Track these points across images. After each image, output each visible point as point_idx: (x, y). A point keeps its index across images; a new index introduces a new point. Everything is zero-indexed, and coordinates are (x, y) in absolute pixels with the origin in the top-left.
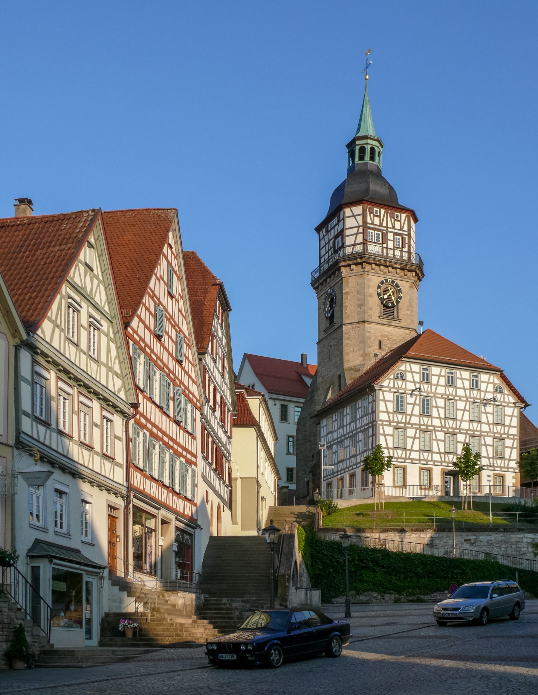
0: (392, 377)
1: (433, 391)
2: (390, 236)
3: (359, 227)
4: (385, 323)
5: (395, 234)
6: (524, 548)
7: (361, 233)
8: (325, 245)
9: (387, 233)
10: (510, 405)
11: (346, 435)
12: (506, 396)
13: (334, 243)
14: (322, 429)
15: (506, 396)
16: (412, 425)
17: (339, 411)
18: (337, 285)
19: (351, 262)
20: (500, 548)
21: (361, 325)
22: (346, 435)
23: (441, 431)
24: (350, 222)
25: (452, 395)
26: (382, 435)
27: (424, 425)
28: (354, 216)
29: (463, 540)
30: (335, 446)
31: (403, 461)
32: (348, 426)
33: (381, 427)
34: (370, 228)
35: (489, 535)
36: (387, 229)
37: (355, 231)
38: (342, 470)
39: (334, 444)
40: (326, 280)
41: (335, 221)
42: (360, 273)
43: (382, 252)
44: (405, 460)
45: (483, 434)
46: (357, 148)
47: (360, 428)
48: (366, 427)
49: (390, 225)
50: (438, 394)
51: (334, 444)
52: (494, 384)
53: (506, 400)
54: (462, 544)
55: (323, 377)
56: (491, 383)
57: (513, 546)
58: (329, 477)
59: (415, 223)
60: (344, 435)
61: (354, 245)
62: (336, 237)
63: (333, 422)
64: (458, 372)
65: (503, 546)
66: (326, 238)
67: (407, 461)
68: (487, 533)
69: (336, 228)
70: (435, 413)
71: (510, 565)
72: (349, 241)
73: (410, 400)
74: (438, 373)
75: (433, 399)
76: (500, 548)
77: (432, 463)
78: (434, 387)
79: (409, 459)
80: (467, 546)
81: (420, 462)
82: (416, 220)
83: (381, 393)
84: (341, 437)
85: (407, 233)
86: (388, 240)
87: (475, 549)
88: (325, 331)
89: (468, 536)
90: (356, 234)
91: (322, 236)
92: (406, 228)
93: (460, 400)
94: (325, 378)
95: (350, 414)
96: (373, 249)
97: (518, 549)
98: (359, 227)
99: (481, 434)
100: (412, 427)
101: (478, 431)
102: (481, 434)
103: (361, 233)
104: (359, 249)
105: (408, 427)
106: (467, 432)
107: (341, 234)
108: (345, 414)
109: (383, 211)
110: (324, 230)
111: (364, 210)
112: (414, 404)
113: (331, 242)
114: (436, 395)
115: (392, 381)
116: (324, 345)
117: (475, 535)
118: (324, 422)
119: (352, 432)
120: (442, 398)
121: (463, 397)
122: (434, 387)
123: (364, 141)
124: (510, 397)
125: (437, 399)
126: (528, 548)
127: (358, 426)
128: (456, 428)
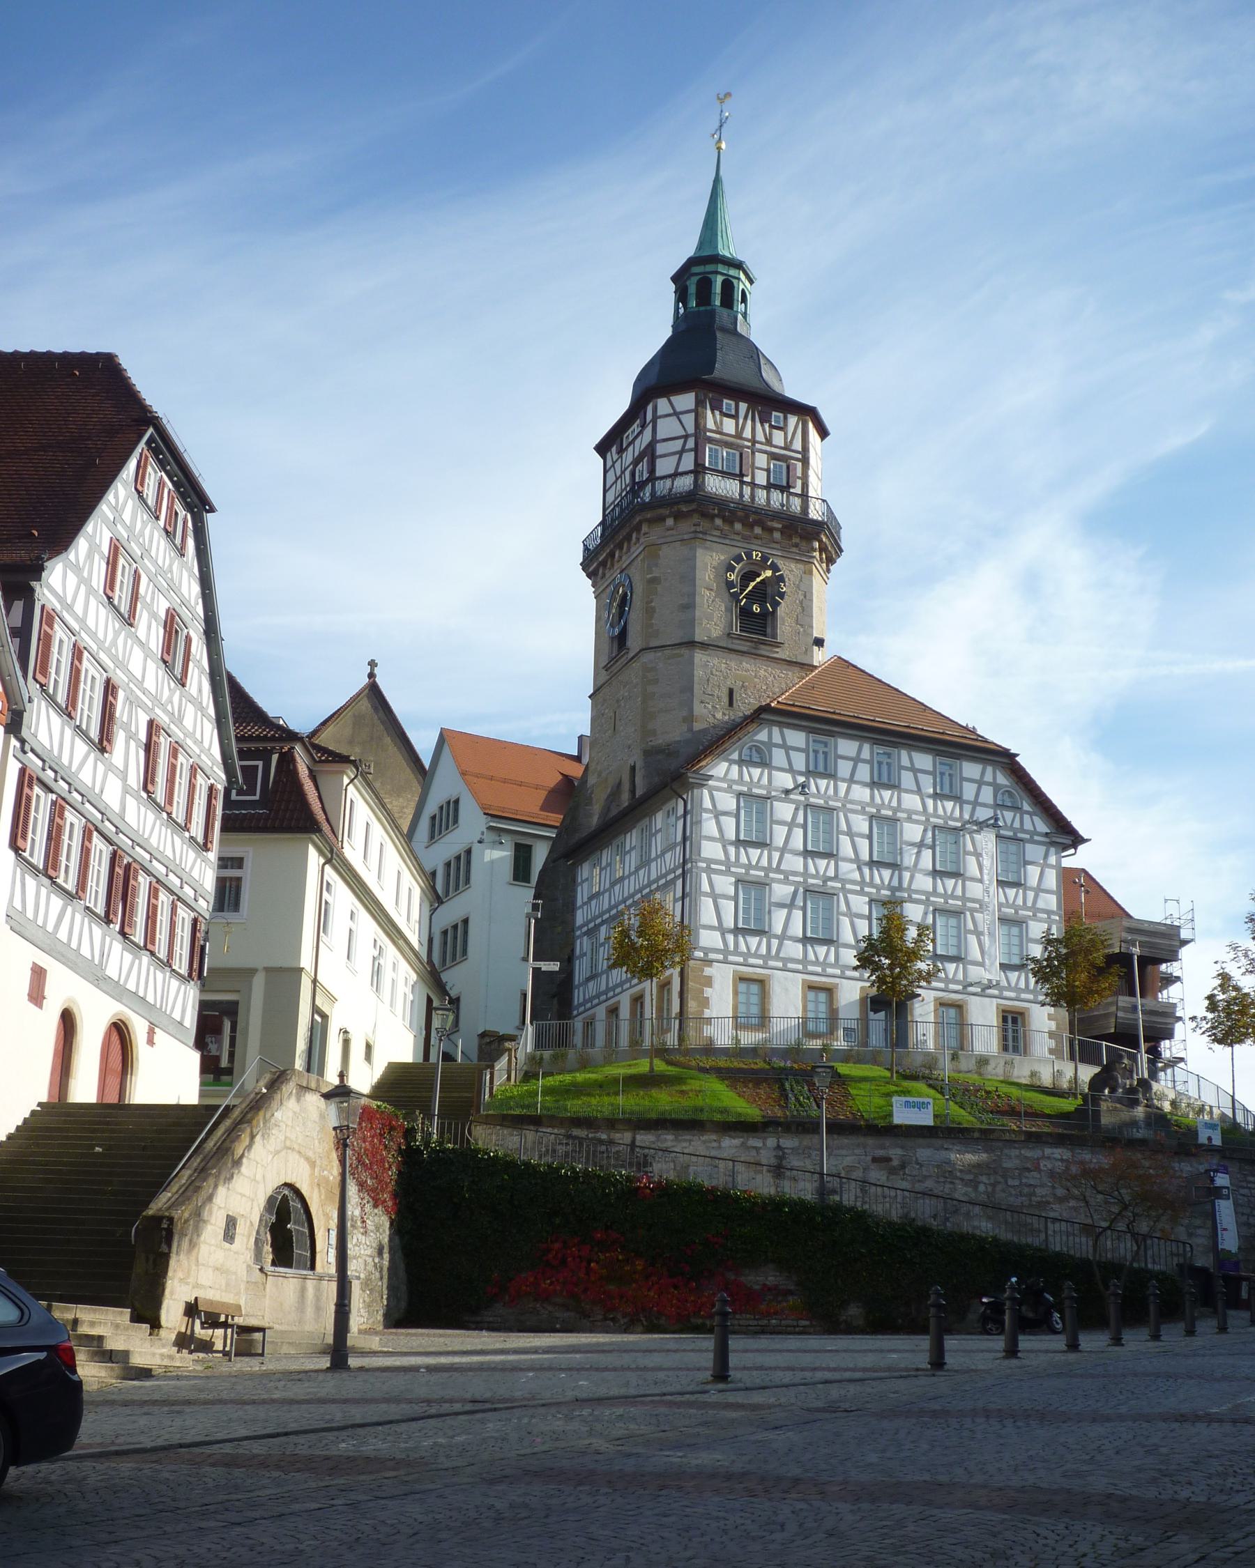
0: (735, 756)
1: (842, 793)
2: (761, 460)
3: (686, 437)
4: (745, 649)
5: (773, 456)
6: (1042, 1186)
7: (691, 450)
8: (616, 482)
9: (753, 453)
10: (1036, 838)
11: (628, 898)
12: (1026, 817)
13: (633, 474)
14: (579, 889)
15: (1026, 817)
16: (787, 874)
17: (615, 843)
18: (635, 563)
19: (666, 512)
20: (975, 1184)
21: (684, 651)
22: (628, 898)
23: (861, 893)
24: (667, 427)
26: (706, 895)
27: (816, 876)
28: (676, 414)
29: (869, 1158)
30: (603, 929)
31: (760, 962)
32: (632, 878)
33: (704, 876)
34: (711, 440)
35: (942, 1148)
36: (753, 445)
37: (678, 445)
38: (617, 986)
39: (603, 923)
40: (612, 555)
41: (636, 427)
42: (686, 537)
43: (741, 495)
44: (765, 962)
45: (969, 904)
46: (695, 279)
47: (656, 881)
48: (669, 878)
49: (760, 437)
50: (852, 802)
51: (603, 923)
52: (997, 788)
53: (1028, 825)
55: (599, 775)
56: (989, 784)
57: (1010, 1182)
58: (589, 1005)
59: (822, 439)
60: (624, 901)
61: (676, 474)
62: (636, 462)
63: (601, 870)
64: (904, 753)
65: (984, 1179)
66: (618, 465)
67: (771, 963)
68: (939, 1142)
69: (637, 442)
71: (1005, 1235)
72: (664, 467)
73: (784, 810)
74: (853, 754)
75: (841, 815)
76: (975, 1184)
77: (838, 972)
79: (777, 958)
80: (877, 1175)
81: (805, 967)
82: (823, 433)
83: (705, 792)
84: (616, 906)
85: (800, 456)
86: (753, 467)
87: (905, 1185)
88: (606, 668)
89: (883, 1147)
90: (681, 453)
91: (609, 463)
92: (797, 445)
93: (909, 819)
94: (604, 775)
95: (638, 849)
96: (716, 485)
97: (1026, 1190)
98: (686, 437)
99: (964, 905)
100: (786, 881)
101: (956, 898)
103: (691, 450)
105: (774, 880)
106: (928, 899)
107: (650, 453)
108: (628, 848)
109: (743, 406)
110: (614, 449)
111: (699, 403)
113: (627, 473)
114: (849, 806)
116: (605, 700)
117: (902, 1147)
118: (584, 871)
119: (640, 891)
120: (863, 812)
121: (917, 813)
123: (709, 268)
124: (1037, 820)
125: (851, 816)
126: (1053, 1187)
127: (653, 876)
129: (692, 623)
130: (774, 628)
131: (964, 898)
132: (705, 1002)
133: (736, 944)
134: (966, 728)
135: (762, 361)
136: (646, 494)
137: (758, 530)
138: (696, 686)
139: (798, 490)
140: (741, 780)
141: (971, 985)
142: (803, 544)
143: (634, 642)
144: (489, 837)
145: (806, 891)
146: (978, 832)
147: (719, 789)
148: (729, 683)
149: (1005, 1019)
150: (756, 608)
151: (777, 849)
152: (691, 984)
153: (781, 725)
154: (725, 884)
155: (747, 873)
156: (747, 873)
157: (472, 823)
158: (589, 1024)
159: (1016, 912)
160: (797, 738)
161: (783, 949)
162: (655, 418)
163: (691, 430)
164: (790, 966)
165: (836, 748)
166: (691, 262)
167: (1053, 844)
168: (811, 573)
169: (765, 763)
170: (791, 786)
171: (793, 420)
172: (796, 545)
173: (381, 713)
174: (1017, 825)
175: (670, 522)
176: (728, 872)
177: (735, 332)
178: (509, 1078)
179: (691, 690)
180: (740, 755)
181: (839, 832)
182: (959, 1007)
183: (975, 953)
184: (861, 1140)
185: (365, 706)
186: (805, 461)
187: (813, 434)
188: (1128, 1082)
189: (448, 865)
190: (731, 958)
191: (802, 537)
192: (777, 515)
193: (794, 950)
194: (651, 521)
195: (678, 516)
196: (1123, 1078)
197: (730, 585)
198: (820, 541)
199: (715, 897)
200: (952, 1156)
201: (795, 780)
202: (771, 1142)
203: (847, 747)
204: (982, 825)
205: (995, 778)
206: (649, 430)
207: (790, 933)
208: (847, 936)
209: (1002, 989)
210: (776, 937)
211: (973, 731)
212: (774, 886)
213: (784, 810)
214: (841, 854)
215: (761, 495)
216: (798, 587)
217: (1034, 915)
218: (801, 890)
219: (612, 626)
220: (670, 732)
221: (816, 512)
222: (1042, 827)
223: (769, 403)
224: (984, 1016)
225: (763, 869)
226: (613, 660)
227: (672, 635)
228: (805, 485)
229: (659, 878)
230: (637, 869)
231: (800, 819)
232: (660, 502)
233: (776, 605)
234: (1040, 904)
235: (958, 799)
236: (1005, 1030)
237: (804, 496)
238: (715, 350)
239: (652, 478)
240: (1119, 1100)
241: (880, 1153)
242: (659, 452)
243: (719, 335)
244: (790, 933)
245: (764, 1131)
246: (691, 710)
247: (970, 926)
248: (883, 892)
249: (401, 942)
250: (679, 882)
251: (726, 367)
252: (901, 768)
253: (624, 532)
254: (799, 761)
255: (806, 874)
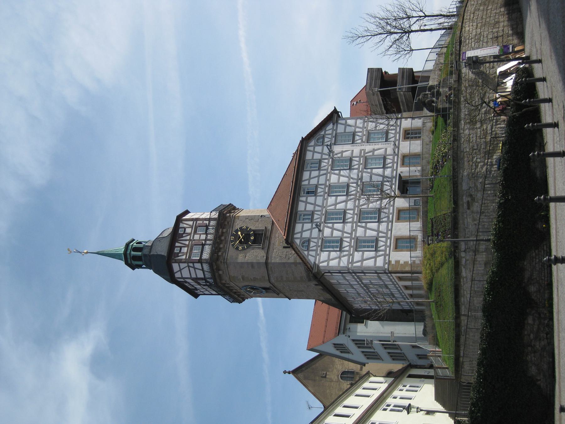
0: (306, 253)
1: (320, 208)
2: (197, 237)
5: (195, 232)
6: (476, 133)
9: (194, 240)
13: (204, 285)
15: (327, 132)
16: (353, 230)
19: (217, 275)
21: (270, 266)
25: (325, 188)
26: (362, 264)
27: (353, 218)
28: (180, 270)
29: (468, 211)
31: (389, 240)
33: (354, 265)
34: (190, 257)
40: (235, 293)
42: (226, 266)
44: (389, 238)
47: (358, 282)
49: (188, 238)
50: (323, 204)
54: (473, 212)
56: (314, 148)
61: (203, 270)
62: (200, 284)
64: (303, 183)
66: (202, 290)
67: (389, 236)
70: (341, 206)
72: (200, 275)
73: (327, 232)
78: (317, 208)
79: (387, 233)
80: (476, 207)
82: (187, 212)
86: (199, 240)
88: (278, 294)
90: (195, 268)
91: (201, 293)
93: (329, 180)
98: (189, 266)
99: (362, 157)
100: (356, 230)
101: (360, 160)
102: (362, 157)
104: (206, 267)
105: (355, 236)
106: (361, 172)
107: (196, 280)
109: (177, 244)
112: (333, 229)
115: (311, 253)
118: (356, 306)
119: (362, 287)
122: (317, 208)
123: (128, 257)
125: (329, 204)
127: (356, 283)
128: (357, 183)
129: (258, 263)
130: (259, 230)
131: (360, 157)
132: (406, 263)
133: (382, 251)
134: (293, 157)
135: (161, 236)
136: (211, 281)
137: (223, 238)
138: (283, 261)
139: (207, 222)
140: (316, 251)
141: (395, 152)
142: (228, 220)
143: (267, 285)
144: (348, 333)
145: (359, 222)
146: (333, 152)
147: (319, 259)
148: (281, 248)
149: (408, 138)
150: (252, 238)
151: (343, 235)
152: (399, 269)
153: (293, 234)
154: (357, 256)
155: (353, 247)
156: (353, 247)
157: (342, 339)
158: (418, 304)
159: (365, 135)
160: (298, 228)
161: (383, 231)
162: (182, 278)
163: (186, 265)
164: (390, 228)
165: (301, 211)
166: (127, 263)
167: (337, 122)
168: (238, 216)
169: (309, 241)
170: (317, 230)
171: (181, 225)
172: (228, 223)
173: (303, 369)
174: (330, 136)
175: (221, 272)
176: (353, 255)
177: (152, 246)
178: (440, 356)
179: (284, 263)
180: (305, 251)
181: (335, 209)
182: (404, 157)
183: (381, 152)
184: (460, 214)
185: (301, 375)
186: (197, 220)
187: (188, 216)
188: (429, 96)
189: (359, 347)
190: (388, 253)
191: (225, 221)
192: (217, 231)
193: (383, 227)
194: (221, 280)
195: (218, 269)
196: (427, 98)
197: (244, 249)
198: (227, 213)
199: (363, 260)
200: (465, 174)
201: (314, 228)
202: (463, 254)
203: (301, 207)
204: (331, 151)
205: (311, 146)
206: (187, 280)
207: (376, 228)
208: (376, 205)
209: (396, 140)
210: (378, 234)
211: (294, 154)
212: (357, 235)
213: (327, 232)
214: (344, 208)
215: (210, 237)
216: (244, 221)
217: (365, 128)
218: (359, 224)
219: (262, 292)
220: (301, 271)
221: (215, 215)
222: (330, 126)
223: (176, 234)
224: (406, 147)
225: (351, 240)
226: (274, 292)
227: (263, 270)
228: (206, 219)
229: (357, 281)
230: (353, 288)
231: (330, 225)
232: (213, 277)
233: (251, 230)
234: (361, 126)
235: (320, 161)
236: (412, 138)
237: (210, 220)
238: (157, 255)
239: (204, 279)
240: (437, 99)
241: (465, 205)
242: (195, 276)
243: (152, 254)
244: (376, 228)
245: (458, 258)
246: (292, 263)
247: (371, 154)
248: (359, 190)
249: (385, 395)
250: (358, 274)
251: (162, 250)
252: (309, 184)
253: (226, 289)
254: (307, 226)
255: (352, 222)
